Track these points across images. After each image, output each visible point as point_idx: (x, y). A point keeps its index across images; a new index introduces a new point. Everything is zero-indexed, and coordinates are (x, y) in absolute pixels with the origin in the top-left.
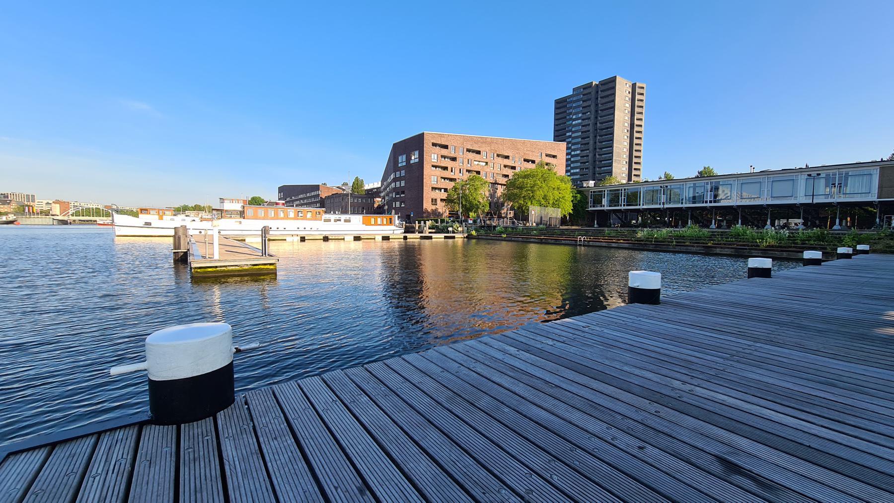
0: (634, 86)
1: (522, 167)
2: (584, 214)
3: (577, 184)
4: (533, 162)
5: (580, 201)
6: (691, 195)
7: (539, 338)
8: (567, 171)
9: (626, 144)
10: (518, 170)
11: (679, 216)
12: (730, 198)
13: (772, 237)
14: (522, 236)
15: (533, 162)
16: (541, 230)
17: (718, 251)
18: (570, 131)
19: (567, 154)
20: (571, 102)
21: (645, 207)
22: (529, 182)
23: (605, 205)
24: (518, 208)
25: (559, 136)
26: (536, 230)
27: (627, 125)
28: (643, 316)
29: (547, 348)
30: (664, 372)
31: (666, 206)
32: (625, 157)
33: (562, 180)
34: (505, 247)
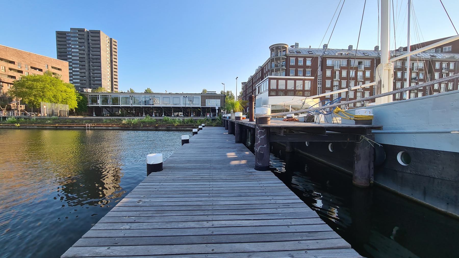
0: (111, 39)
1: (28, 72)
2: (83, 107)
3: (79, 89)
4: (41, 70)
5: (82, 101)
6: (144, 100)
7: (116, 226)
8: (70, 80)
9: (109, 70)
10: (25, 74)
11: (138, 111)
12: (159, 103)
13: (178, 122)
14: (34, 124)
15: (41, 70)
16: (54, 119)
17: (160, 128)
18: (71, 55)
19: (70, 69)
20: (69, 36)
21: (122, 106)
22: (39, 85)
23: (100, 103)
24: (29, 103)
25: (62, 55)
26: (49, 119)
27: (109, 60)
28: (166, 181)
29: (128, 233)
30: (196, 218)
31: (133, 106)
32: (109, 77)
33: (68, 86)
34: (18, 135)
